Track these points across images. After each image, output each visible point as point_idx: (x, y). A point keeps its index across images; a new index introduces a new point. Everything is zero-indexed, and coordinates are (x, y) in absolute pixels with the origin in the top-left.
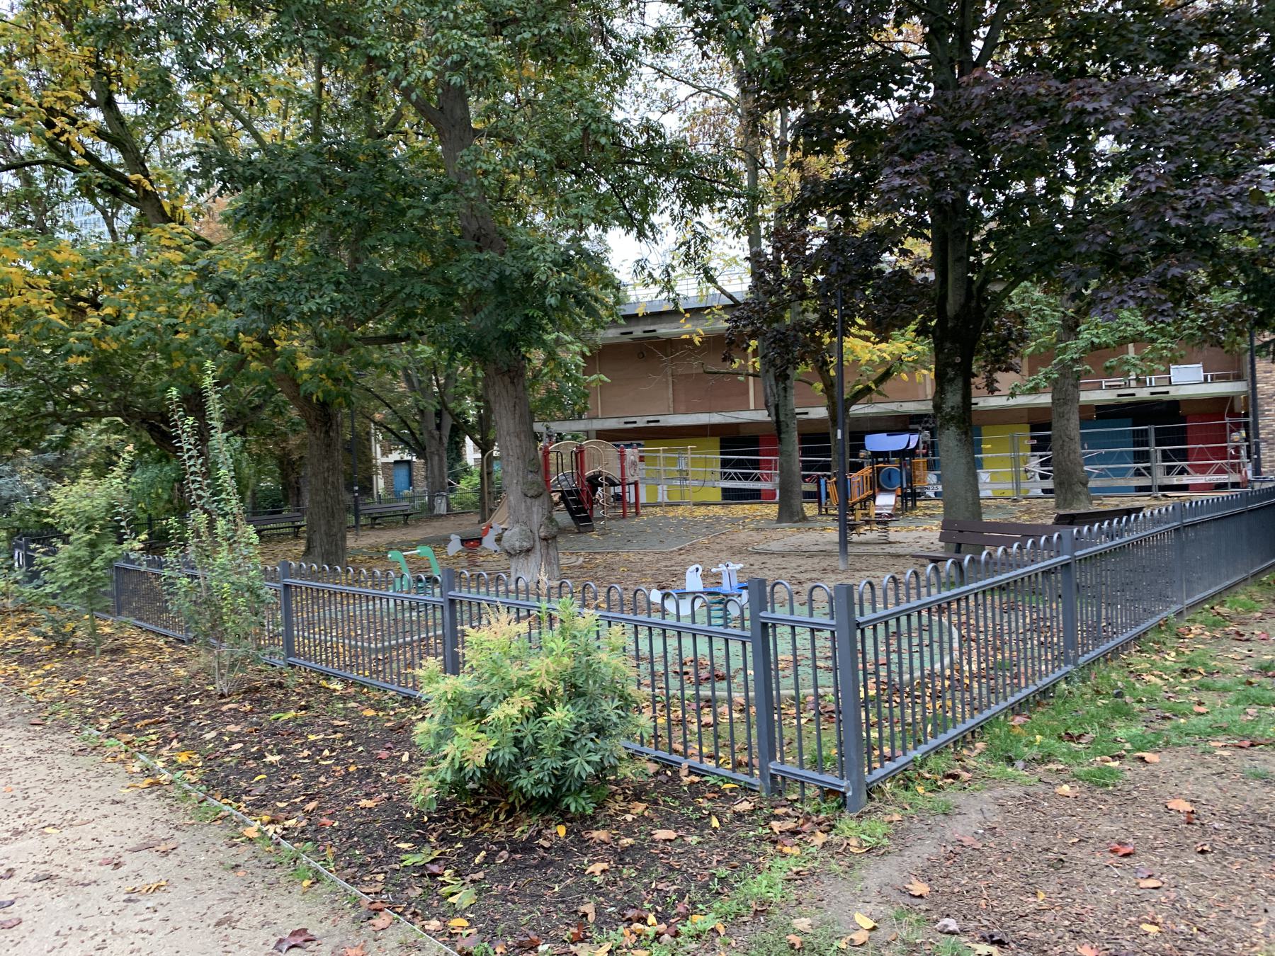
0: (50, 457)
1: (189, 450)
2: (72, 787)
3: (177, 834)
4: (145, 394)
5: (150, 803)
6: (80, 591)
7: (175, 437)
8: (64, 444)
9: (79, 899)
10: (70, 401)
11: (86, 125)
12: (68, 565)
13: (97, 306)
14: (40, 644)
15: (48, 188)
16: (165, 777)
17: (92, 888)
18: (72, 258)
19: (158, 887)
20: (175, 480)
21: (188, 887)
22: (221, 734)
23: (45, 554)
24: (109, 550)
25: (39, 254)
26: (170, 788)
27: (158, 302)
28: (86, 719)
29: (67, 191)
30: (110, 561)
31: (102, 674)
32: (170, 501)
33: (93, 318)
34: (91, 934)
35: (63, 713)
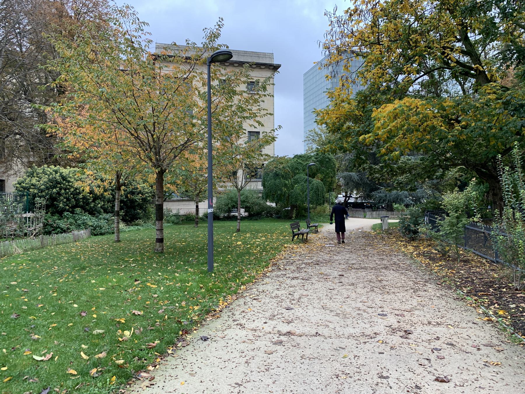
0: (435, 181)
1: (505, 181)
2: (456, 312)
3: (503, 345)
4: (475, 156)
5: (489, 328)
6: (453, 236)
7: (499, 176)
8: (442, 176)
9: (465, 357)
10: (445, 160)
11: (457, 50)
12: (449, 225)
13: (459, 122)
14: (436, 254)
15: (439, 78)
16: (494, 319)
17: (469, 355)
18: (450, 104)
19: (497, 364)
20: (485, 192)
21: (511, 369)
22: (517, 306)
23: (440, 220)
24: (464, 220)
25: (438, 104)
26: (497, 324)
27: (484, 118)
28: (457, 287)
29: (446, 77)
30: (464, 226)
31: (462, 270)
32: (482, 201)
33: (458, 127)
34: (472, 373)
35: (448, 283)
